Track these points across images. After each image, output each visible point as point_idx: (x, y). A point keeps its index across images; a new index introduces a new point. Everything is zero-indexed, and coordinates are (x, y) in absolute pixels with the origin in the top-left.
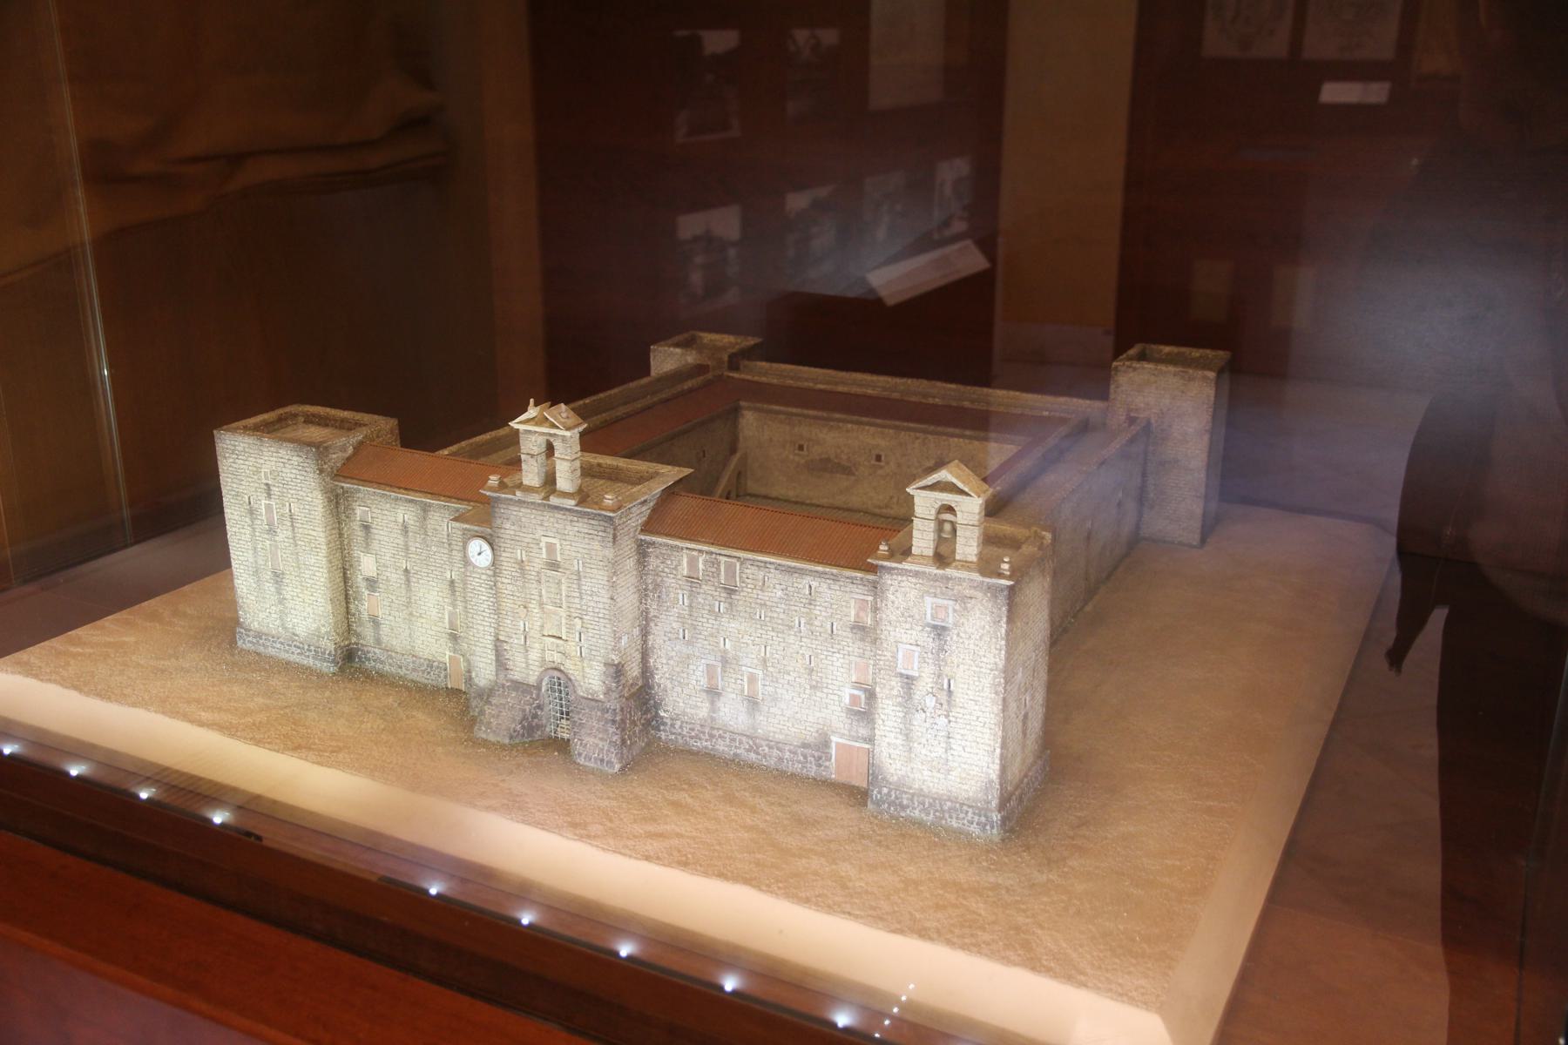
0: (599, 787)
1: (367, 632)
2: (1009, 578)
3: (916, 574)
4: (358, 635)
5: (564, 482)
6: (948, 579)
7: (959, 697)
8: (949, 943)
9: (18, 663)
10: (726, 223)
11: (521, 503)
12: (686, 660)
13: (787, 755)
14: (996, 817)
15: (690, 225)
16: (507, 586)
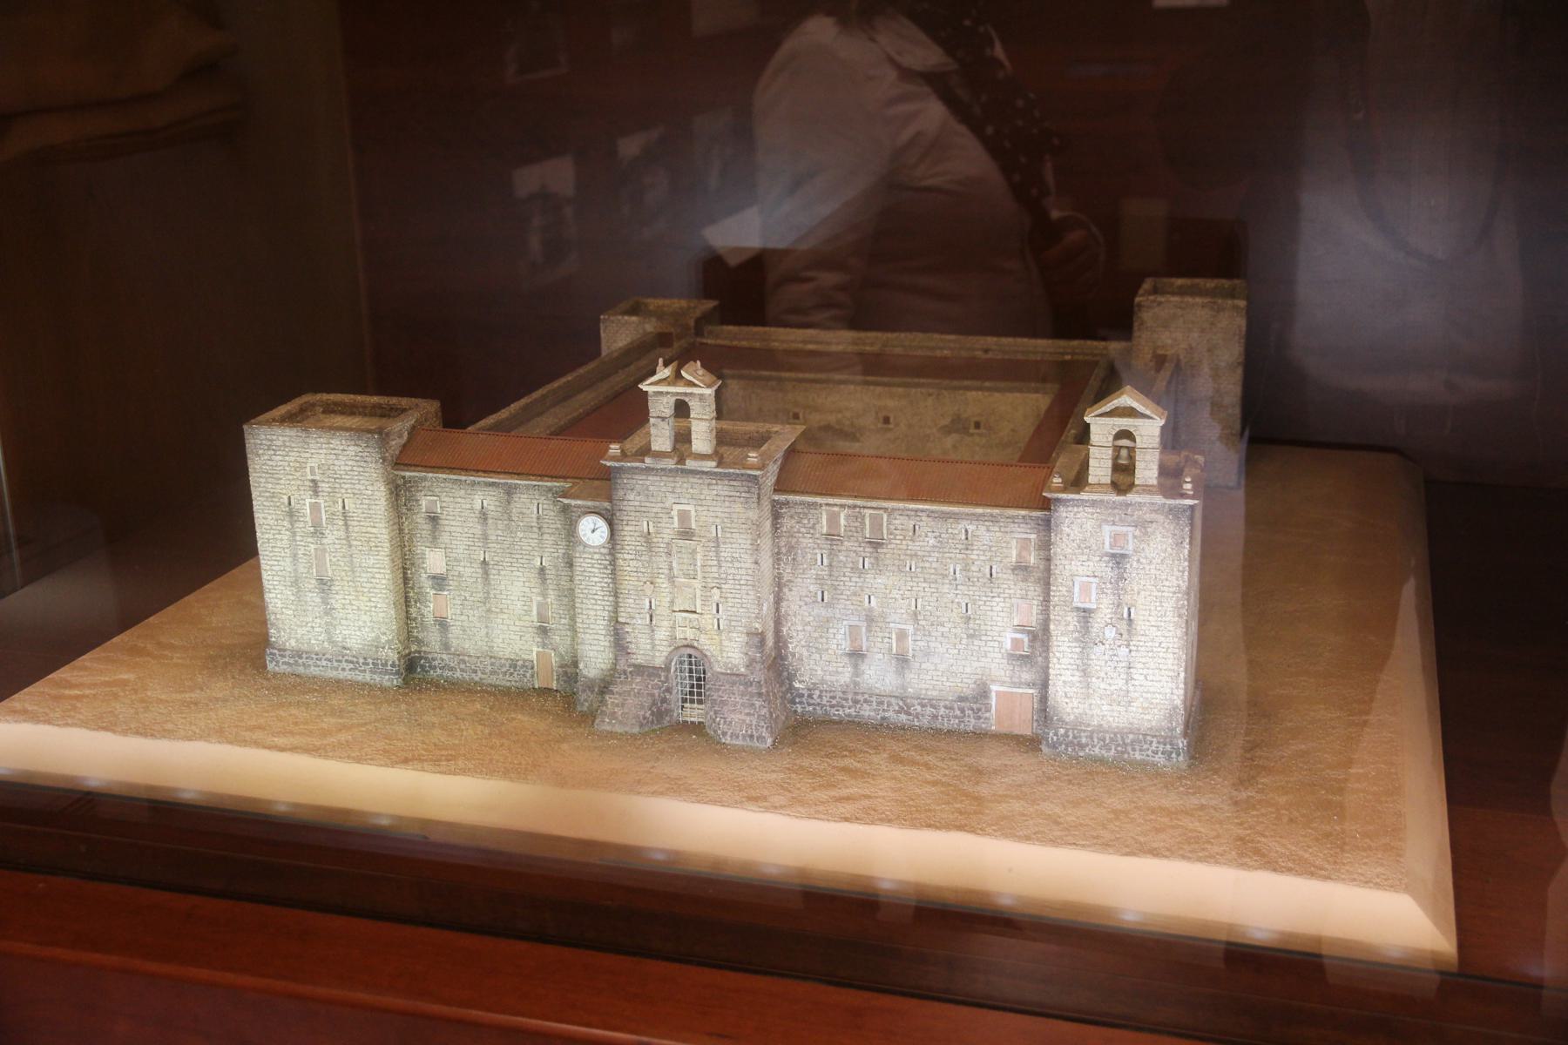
0: (757, 762)
1: (433, 639)
2: (1192, 497)
3: (1094, 504)
4: (419, 642)
5: (702, 441)
6: (1128, 505)
7: (1140, 625)
8: (1184, 857)
9: (14, 712)
10: (557, 175)
11: (649, 470)
12: (825, 624)
13: (942, 711)
14: (1182, 743)
15: (527, 180)
16: (628, 561)
